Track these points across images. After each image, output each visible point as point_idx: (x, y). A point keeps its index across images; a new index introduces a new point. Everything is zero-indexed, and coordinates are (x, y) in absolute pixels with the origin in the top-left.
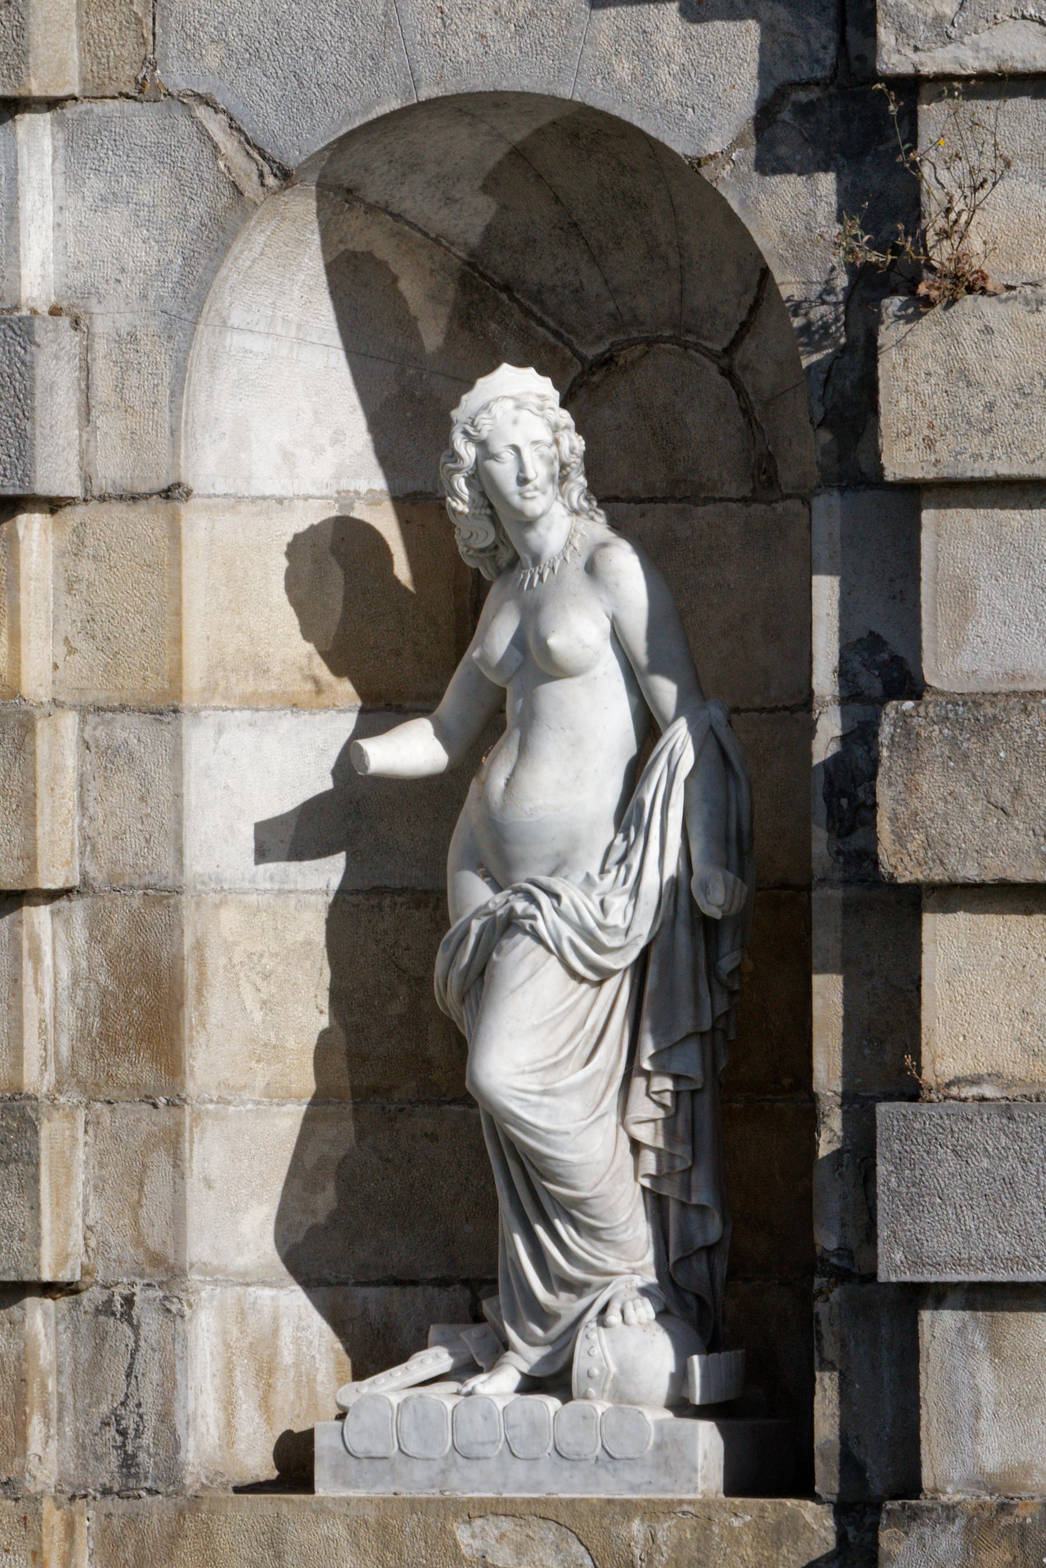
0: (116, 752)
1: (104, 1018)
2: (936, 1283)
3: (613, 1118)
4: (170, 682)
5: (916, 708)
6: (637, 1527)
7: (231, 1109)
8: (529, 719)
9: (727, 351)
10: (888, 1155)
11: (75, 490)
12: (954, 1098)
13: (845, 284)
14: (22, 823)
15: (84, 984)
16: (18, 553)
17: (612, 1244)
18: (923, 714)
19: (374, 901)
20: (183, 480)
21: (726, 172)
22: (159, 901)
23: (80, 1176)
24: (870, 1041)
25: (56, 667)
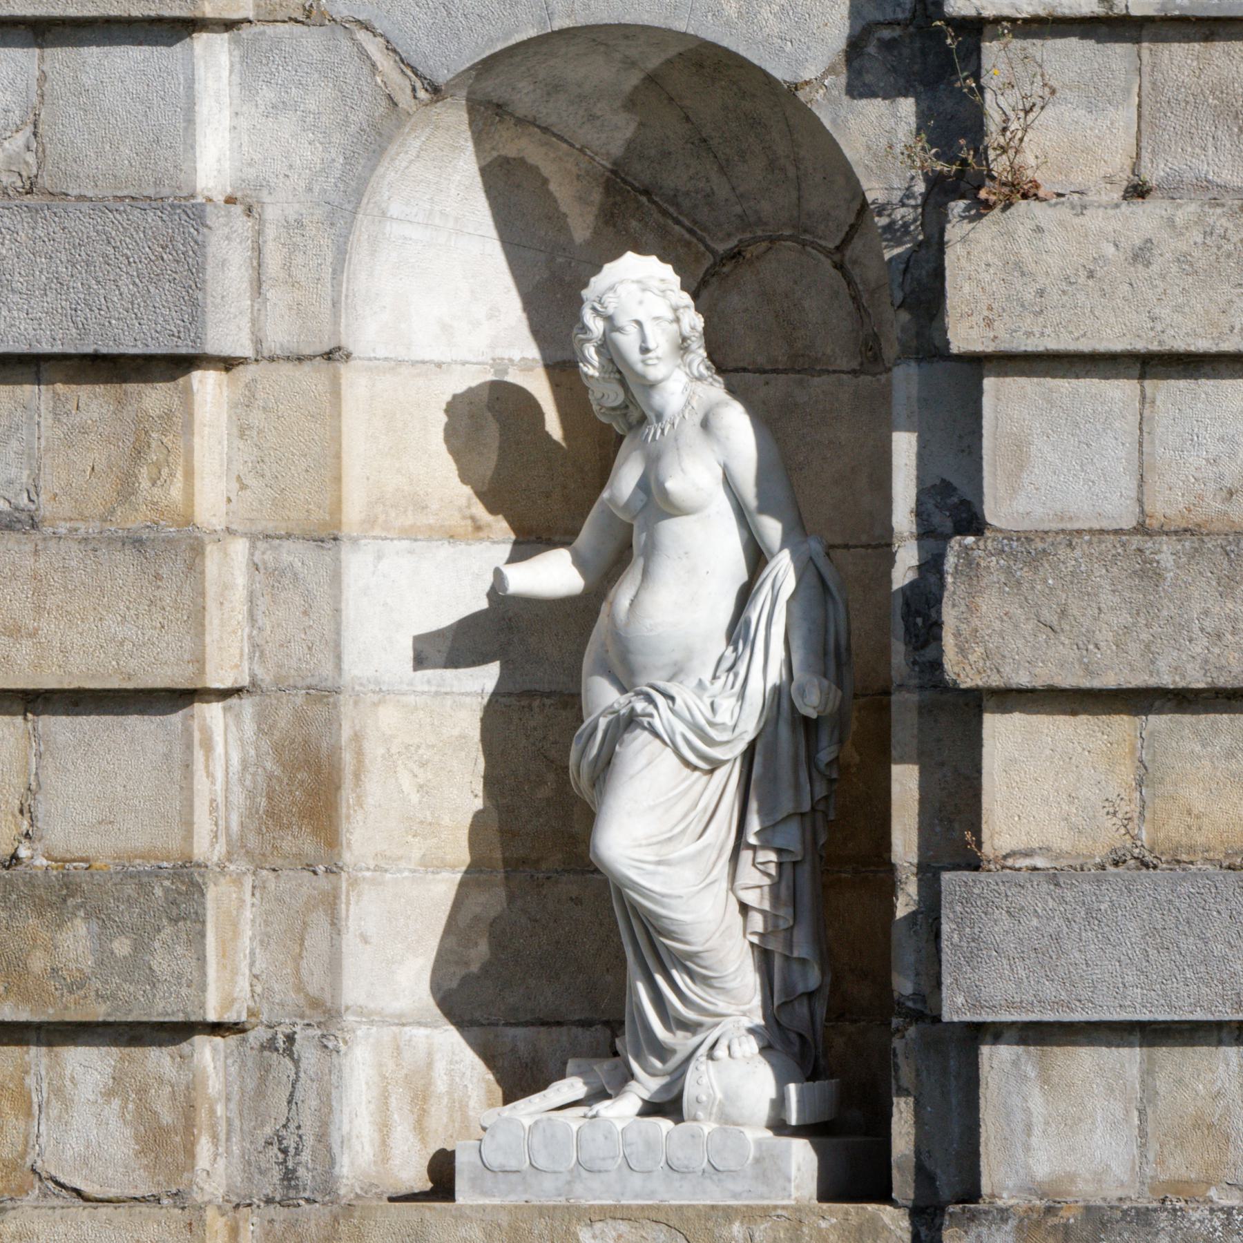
0: (283, 573)
1: (270, 798)
2: (993, 1023)
3: (724, 884)
4: (331, 514)
5: (976, 542)
6: (737, 1229)
7: (388, 876)
8: (651, 550)
9: (838, 249)
10: (951, 915)
11: (248, 352)
12: (1010, 868)
13: (923, 190)
14: (192, 632)
15: (252, 770)
16: (192, 404)
17: (723, 991)
18: (982, 547)
19: (525, 702)
20: (343, 344)
21: (819, 95)
22: (320, 700)
23: (247, 932)
24: (941, 820)
25: (229, 500)
